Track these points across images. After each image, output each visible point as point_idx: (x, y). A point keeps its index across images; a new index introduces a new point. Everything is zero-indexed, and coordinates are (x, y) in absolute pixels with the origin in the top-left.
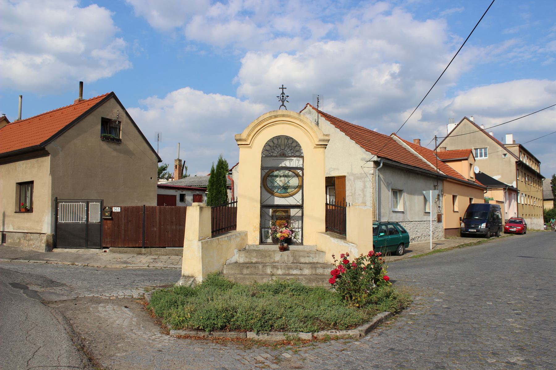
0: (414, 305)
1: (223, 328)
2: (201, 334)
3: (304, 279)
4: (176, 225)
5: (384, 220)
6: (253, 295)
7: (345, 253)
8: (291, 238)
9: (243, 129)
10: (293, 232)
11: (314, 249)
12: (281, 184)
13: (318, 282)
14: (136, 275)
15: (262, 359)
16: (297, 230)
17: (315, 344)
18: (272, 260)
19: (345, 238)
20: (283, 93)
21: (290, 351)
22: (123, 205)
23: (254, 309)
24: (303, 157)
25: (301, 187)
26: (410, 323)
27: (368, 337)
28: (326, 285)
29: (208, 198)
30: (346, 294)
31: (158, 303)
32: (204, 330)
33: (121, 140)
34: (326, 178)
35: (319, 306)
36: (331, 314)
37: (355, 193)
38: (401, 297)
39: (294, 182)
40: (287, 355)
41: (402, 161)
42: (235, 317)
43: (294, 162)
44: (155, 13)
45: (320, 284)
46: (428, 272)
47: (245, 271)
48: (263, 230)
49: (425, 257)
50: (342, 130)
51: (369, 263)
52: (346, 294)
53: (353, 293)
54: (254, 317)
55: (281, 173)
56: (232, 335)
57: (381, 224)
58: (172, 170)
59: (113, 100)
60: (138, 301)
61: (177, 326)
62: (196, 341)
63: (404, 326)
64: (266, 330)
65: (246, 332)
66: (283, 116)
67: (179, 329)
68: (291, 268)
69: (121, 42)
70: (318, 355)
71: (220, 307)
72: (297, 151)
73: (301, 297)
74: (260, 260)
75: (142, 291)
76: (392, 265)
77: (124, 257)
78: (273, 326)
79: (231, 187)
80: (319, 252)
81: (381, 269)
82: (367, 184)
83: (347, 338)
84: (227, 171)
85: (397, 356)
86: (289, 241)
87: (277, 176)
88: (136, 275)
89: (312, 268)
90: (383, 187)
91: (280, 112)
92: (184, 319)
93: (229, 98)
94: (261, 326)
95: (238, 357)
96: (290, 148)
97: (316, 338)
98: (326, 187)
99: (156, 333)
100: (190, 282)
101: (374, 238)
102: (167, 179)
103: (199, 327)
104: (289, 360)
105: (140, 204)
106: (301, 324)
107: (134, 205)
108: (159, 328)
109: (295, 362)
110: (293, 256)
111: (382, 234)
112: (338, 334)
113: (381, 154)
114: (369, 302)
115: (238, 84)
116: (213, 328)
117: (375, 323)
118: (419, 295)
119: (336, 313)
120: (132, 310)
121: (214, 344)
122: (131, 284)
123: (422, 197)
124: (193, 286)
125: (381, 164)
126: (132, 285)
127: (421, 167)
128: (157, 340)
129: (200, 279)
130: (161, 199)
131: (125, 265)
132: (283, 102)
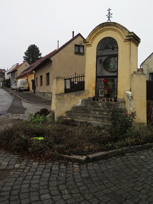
20: (109, 13)
59: (80, 37)
96: (111, 44)
132: (109, 18)
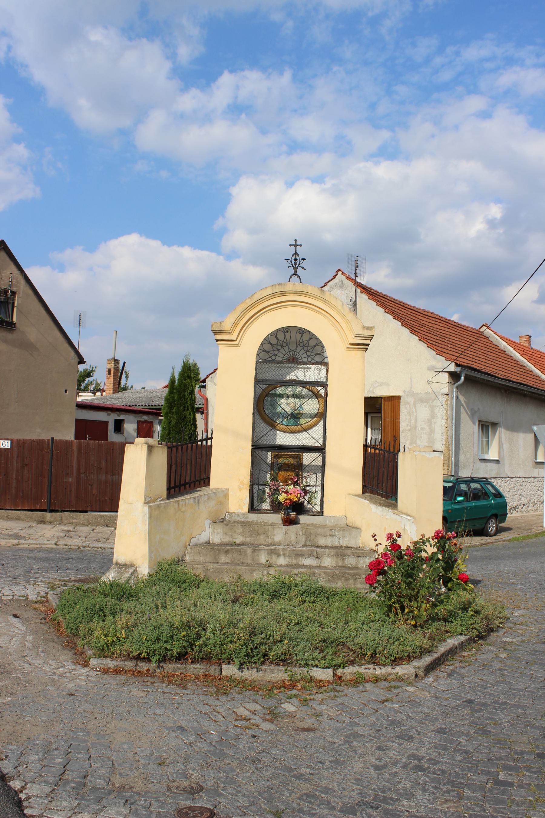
0: (511, 625)
1: (181, 657)
2: (144, 666)
3: (323, 575)
4: (107, 473)
5: (464, 473)
6: (235, 600)
7: (394, 533)
8: (302, 503)
9: (232, 307)
10: (306, 492)
11: (342, 523)
12: (288, 409)
13: (347, 580)
14: (34, 559)
15: (246, 713)
16: (313, 489)
17: (338, 688)
18: (270, 541)
19: (393, 505)
20: (296, 254)
21: (294, 700)
22: (16, 437)
23: (235, 625)
24: (326, 365)
25: (322, 415)
26: (503, 656)
27: (430, 680)
28: (361, 586)
29: (164, 428)
30: (394, 603)
31: (71, 610)
32: (148, 659)
33: (15, 324)
34: (365, 398)
35: (346, 623)
36: (367, 637)
37: (416, 427)
38: (489, 611)
39: (311, 406)
40: (289, 707)
41: (499, 373)
42: (203, 639)
43: (312, 373)
44: (83, 102)
45: (350, 584)
46: (538, 567)
47: (223, 558)
48: (256, 488)
49: (533, 540)
50: (397, 316)
51: (435, 550)
52: (394, 603)
53: (407, 601)
54: (235, 640)
55: (289, 390)
56: (197, 669)
57: (458, 481)
58: (101, 376)
60: (37, 606)
61: (103, 652)
62: (133, 679)
63: (492, 661)
64: (255, 663)
65: (220, 664)
66: (295, 293)
67: (106, 657)
68: (302, 555)
69: (21, 151)
70: (342, 707)
71: (177, 621)
72: (317, 354)
73: (317, 606)
74: (248, 540)
75: (43, 588)
76: (475, 553)
77: (15, 527)
78: (267, 655)
79: (203, 410)
80: (351, 528)
81: (456, 560)
82: (436, 411)
83: (394, 680)
84: (198, 380)
85: (477, 715)
86: (298, 508)
87: (281, 396)
88: (34, 559)
89: (337, 555)
90: (465, 418)
91: (290, 287)
92: (115, 639)
93: (205, 254)
94: (247, 655)
95: (206, 709)
96: (306, 349)
97: (340, 678)
98: (366, 414)
99: (65, 663)
100: (127, 575)
101: (444, 505)
102: (94, 392)
103: (140, 654)
104: (292, 716)
105: (45, 436)
106: (316, 654)
107: (35, 437)
108: (70, 654)
109: (303, 720)
110: (305, 534)
111: (460, 499)
112: (378, 671)
113: (464, 361)
114: (434, 618)
115: (224, 231)
116: (164, 656)
117: (442, 655)
118: (519, 608)
119: (376, 636)
120: (24, 621)
121: (165, 685)
122: (25, 576)
123: (532, 436)
124: (131, 582)
125: (463, 378)
126: (28, 577)
127: (530, 383)
128: (68, 675)
129: (144, 570)
130: (83, 428)
131: (16, 541)
132: (296, 269)
